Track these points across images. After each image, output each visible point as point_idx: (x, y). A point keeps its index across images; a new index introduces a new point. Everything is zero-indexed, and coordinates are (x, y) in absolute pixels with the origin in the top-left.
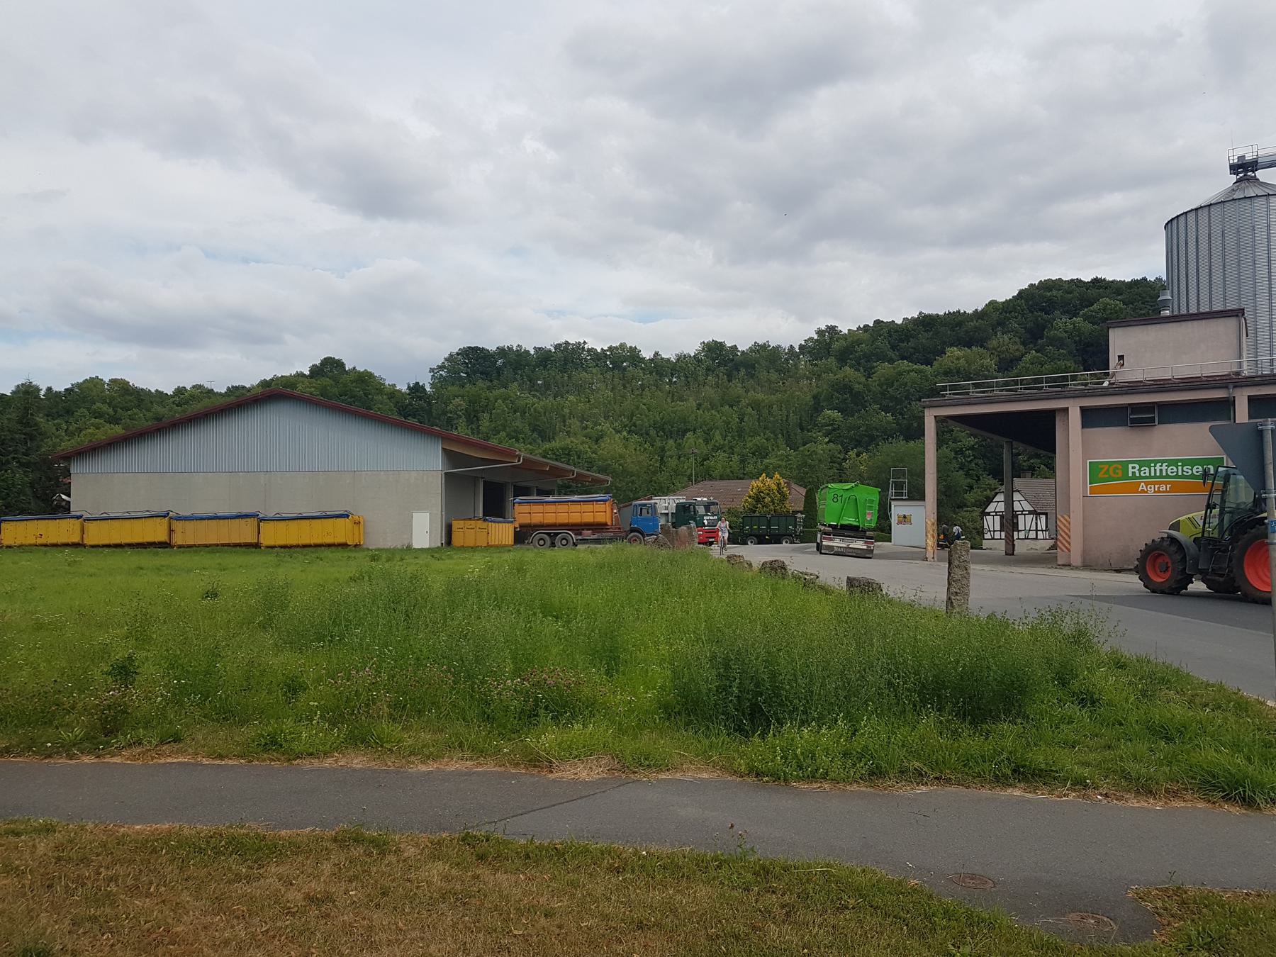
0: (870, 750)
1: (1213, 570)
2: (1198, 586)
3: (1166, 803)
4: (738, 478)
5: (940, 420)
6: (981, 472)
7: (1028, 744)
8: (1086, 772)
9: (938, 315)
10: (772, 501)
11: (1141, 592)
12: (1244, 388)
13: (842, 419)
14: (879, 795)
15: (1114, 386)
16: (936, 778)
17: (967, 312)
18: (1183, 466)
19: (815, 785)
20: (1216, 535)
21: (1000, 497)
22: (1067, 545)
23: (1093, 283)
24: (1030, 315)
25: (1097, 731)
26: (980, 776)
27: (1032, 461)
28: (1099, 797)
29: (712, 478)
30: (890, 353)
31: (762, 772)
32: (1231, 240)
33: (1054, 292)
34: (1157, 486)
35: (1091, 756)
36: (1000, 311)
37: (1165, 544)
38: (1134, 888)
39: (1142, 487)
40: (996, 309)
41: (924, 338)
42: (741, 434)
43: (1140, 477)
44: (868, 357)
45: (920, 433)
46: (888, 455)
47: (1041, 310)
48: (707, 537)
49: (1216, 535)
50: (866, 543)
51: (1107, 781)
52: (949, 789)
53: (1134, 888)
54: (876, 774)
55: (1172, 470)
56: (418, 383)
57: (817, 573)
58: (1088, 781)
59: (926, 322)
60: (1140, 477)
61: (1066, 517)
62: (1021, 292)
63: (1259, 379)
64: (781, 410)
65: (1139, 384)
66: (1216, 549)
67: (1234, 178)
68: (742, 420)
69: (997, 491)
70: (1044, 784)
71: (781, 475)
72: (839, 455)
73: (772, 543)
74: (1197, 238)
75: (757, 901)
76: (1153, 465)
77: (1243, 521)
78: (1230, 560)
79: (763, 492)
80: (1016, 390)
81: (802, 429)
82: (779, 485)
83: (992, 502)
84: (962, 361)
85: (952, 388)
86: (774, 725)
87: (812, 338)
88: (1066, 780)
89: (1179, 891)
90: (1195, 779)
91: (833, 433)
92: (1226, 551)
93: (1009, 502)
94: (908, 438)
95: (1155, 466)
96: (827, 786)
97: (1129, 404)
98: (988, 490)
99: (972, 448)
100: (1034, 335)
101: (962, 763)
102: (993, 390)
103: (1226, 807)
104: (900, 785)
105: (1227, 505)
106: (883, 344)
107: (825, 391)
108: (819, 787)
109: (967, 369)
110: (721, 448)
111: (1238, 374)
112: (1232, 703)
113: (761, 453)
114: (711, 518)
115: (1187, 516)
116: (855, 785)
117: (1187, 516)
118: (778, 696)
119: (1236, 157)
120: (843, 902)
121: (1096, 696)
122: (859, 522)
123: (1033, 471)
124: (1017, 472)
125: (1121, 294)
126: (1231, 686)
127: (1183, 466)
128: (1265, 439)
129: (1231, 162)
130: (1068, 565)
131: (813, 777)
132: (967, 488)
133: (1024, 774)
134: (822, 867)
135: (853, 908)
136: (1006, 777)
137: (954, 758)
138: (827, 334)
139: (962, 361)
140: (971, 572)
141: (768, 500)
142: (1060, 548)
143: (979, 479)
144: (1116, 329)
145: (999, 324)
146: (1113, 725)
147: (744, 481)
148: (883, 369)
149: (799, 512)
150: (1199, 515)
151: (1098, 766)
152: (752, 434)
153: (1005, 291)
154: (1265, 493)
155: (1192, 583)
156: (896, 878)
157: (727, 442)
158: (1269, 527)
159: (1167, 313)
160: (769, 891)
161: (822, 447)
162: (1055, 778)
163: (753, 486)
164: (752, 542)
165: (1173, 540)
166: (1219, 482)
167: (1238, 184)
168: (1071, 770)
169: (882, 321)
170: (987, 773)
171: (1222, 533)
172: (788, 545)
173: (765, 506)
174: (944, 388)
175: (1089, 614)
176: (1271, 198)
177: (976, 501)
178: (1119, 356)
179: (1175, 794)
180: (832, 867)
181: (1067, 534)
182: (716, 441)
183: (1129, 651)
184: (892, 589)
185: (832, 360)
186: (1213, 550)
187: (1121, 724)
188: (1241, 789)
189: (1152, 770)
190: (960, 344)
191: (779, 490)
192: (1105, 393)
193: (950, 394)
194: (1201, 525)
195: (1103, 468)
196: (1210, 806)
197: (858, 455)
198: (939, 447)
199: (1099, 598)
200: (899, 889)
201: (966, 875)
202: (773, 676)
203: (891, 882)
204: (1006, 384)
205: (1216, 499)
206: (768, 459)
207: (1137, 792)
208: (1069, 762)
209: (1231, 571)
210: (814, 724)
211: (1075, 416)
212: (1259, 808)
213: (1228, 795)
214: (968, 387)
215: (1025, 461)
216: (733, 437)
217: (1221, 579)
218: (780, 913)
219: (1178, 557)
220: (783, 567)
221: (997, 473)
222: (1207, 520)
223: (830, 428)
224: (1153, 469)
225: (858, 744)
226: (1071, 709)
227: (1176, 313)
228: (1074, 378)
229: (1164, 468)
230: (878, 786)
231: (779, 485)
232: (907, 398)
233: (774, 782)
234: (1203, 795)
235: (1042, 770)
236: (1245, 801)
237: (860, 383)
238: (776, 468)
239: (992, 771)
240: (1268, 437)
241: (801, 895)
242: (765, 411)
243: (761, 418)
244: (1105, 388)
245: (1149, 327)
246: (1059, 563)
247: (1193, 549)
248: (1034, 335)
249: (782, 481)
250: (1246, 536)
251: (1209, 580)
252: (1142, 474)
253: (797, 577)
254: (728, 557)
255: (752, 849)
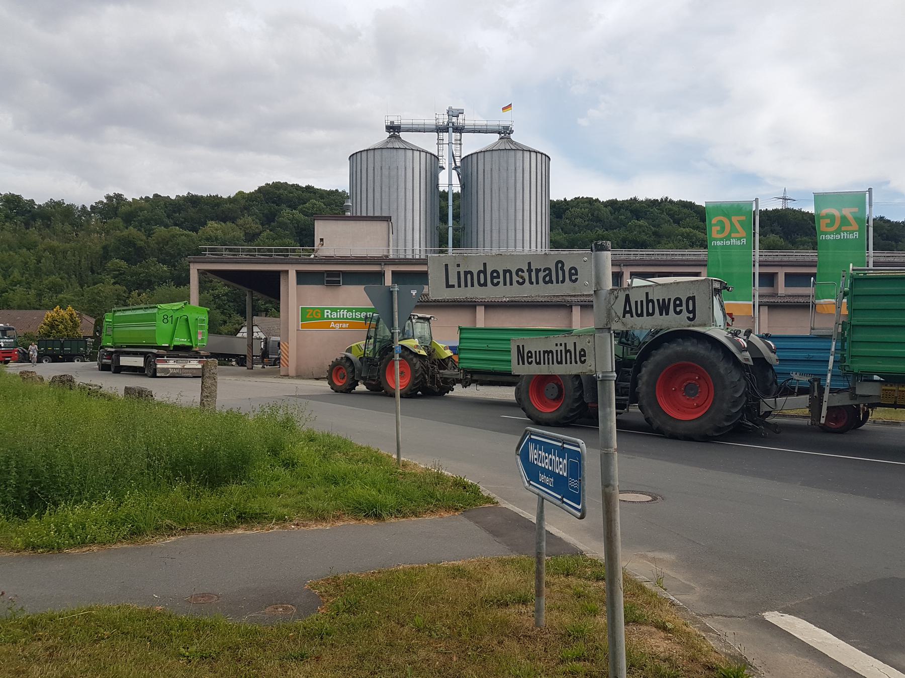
0: (132, 516)
1: (369, 377)
2: (361, 387)
3: (333, 524)
4: (34, 309)
5: (202, 273)
6: (232, 312)
7: (248, 497)
8: (285, 511)
9: (202, 197)
10: (66, 328)
11: (328, 392)
12: (628, 267)
13: (127, 267)
14: (138, 548)
15: (317, 258)
16: (183, 530)
17: (223, 197)
18: (356, 312)
19: (85, 549)
20: (371, 355)
21: (244, 330)
22: (286, 362)
23: (306, 189)
24: (266, 205)
25: (294, 483)
26: (214, 524)
27: (267, 305)
28: (293, 526)
29: (9, 307)
30: (166, 220)
31: (38, 546)
32: (385, 172)
33: (281, 191)
34: (341, 324)
35: (289, 500)
36: (246, 199)
37: (343, 361)
38: (309, 582)
39: (332, 325)
40: (244, 198)
41: (192, 212)
42: (38, 272)
43: (332, 319)
44: (148, 221)
45: (186, 281)
46: (164, 296)
47: (273, 202)
48: (3, 357)
49: (371, 355)
50: (199, 362)
51: (299, 515)
52: (192, 536)
53: (309, 582)
54: (136, 533)
55: (349, 315)
56: (92, 205)
57: (100, 385)
58: (286, 517)
59: (193, 201)
60: (332, 319)
61: (287, 344)
62: (260, 189)
63: (398, 261)
64: (75, 256)
65: (332, 258)
66: (371, 364)
67: (388, 135)
68: (39, 262)
69: (243, 325)
70: (258, 523)
71: (73, 307)
72: (124, 295)
73: (65, 362)
74: (367, 169)
75: (23, 651)
76: (338, 311)
77: (386, 347)
78: (379, 371)
79: (57, 321)
80: (271, 256)
81: (93, 272)
82: (71, 315)
83: (239, 332)
84: (219, 232)
85: (211, 250)
86: (50, 507)
87: (102, 202)
88: (272, 519)
89: (336, 578)
90: (350, 507)
91: (119, 277)
92: (377, 365)
93: (251, 333)
94: (178, 284)
95: (340, 312)
96: (95, 548)
97: (326, 271)
98: (237, 325)
99: (226, 295)
100: (269, 219)
101: (202, 516)
102: (223, 254)
103: (366, 522)
104: (154, 539)
105: (378, 337)
106: (160, 212)
107: (113, 244)
108: (88, 550)
109: (223, 237)
110: (20, 283)
111: (387, 256)
112: (374, 458)
113: (56, 289)
114: (7, 341)
115: (356, 344)
116: (119, 544)
117: (356, 344)
118: (55, 483)
119: (389, 121)
120: (100, 635)
121: (295, 461)
122: (191, 341)
123: (267, 312)
124: (256, 312)
125: (324, 199)
126: (374, 448)
127: (356, 312)
128: (394, 297)
129: (387, 124)
130: (287, 376)
131: (83, 543)
132: (221, 322)
133: (245, 518)
134: (84, 612)
135: (108, 638)
136: (233, 522)
137: (196, 513)
138: (114, 200)
139: (219, 232)
140: (218, 381)
141: (61, 327)
142: (282, 365)
143: (231, 317)
144: (319, 221)
145: (246, 209)
146: (304, 478)
147: (40, 312)
148: (160, 231)
149: (89, 337)
150: (362, 343)
151: (293, 507)
152: (48, 273)
153: (250, 186)
154: (393, 330)
155: (358, 385)
156: (145, 607)
157: (24, 278)
158: (395, 350)
159: (348, 214)
160: (35, 640)
161: (108, 288)
162: (265, 518)
163: (48, 315)
164: (46, 361)
165: (348, 359)
166: (374, 323)
167: (390, 139)
168: (276, 511)
169: (160, 196)
170: (219, 521)
171: (375, 354)
172: (79, 363)
173: (59, 332)
174: (205, 250)
175: (294, 407)
176: (407, 150)
177: (228, 332)
178: (321, 239)
179: (338, 518)
180: (92, 610)
181: (286, 355)
182: (14, 277)
183: (319, 429)
184: (365, 387)
185: (118, 220)
186: (370, 365)
187: (309, 477)
188: (374, 510)
189: (326, 504)
190: (217, 219)
191: (72, 319)
192: (311, 262)
193: (209, 254)
194: (363, 349)
195: (309, 312)
196: (358, 522)
197: (139, 295)
198: (200, 292)
199: (300, 396)
200: (147, 615)
201: (199, 595)
202: (51, 466)
203: (140, 612)
204: (250, 250)
205: (372, 334)
206: (62, 294)
207: (316, 520)
208: (275, 506)
209: (379, 378)
210: (85, 501)
211: (292, 276)
212: (384, 520)
213: (367, 514)
214: (221, 250)
215: (262, 305)
216: (31, 275)
217: (374, 383)
218: (42, 654)
219: (350, 369)
220: (71, 380)
221: (243, 313)
222: (367, 346)
223: (117, 273)
224: (338, 313)
225: (122, 513)
226: (280, 471)
227: (354, 215)
228: (294, 251)
229: (345, 313)
230: (138, 542)
231: (71, 315)
232: (179, 254)
233: (48, 551)
234: (354, 516)
235: (257, 514)
236: (376, 517)
237: (142, 240)
238: (69, 302)
239: (223, 519)
240: (395, 295)
241: (64, 637)
242: (60, 256)
243: (56, 261)
244: (311, 259)
245: (339, 222)
246: (282, 374)
247: (358, 364)
248: (269, 219)
249: (74, 312)
250: (387, 356)
251: (367, 383)
252: (333, 317)
253: (82, 388)
254: (21, 373)
255: (22, 609)
